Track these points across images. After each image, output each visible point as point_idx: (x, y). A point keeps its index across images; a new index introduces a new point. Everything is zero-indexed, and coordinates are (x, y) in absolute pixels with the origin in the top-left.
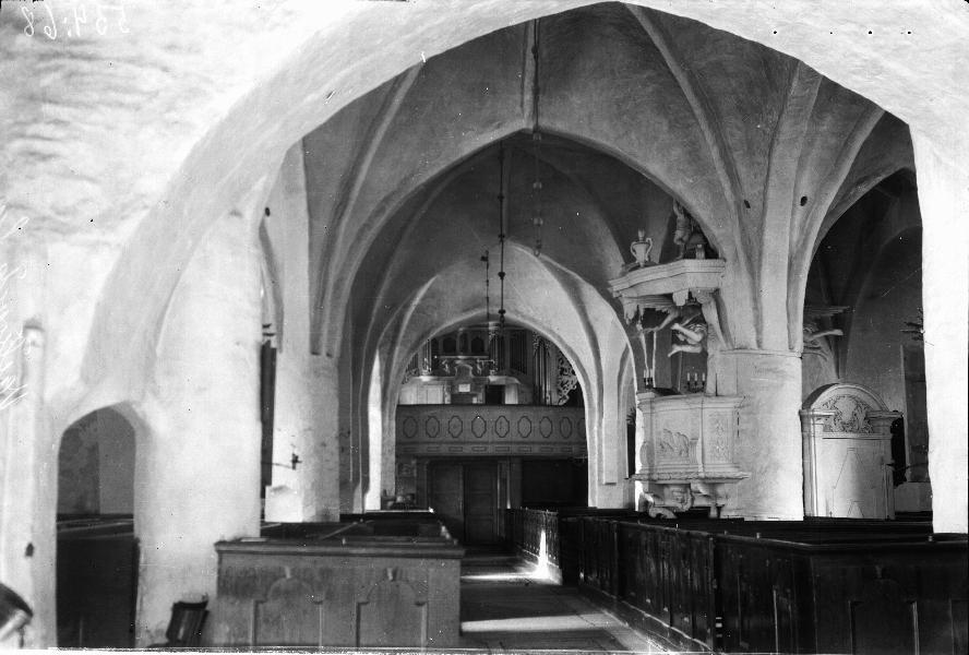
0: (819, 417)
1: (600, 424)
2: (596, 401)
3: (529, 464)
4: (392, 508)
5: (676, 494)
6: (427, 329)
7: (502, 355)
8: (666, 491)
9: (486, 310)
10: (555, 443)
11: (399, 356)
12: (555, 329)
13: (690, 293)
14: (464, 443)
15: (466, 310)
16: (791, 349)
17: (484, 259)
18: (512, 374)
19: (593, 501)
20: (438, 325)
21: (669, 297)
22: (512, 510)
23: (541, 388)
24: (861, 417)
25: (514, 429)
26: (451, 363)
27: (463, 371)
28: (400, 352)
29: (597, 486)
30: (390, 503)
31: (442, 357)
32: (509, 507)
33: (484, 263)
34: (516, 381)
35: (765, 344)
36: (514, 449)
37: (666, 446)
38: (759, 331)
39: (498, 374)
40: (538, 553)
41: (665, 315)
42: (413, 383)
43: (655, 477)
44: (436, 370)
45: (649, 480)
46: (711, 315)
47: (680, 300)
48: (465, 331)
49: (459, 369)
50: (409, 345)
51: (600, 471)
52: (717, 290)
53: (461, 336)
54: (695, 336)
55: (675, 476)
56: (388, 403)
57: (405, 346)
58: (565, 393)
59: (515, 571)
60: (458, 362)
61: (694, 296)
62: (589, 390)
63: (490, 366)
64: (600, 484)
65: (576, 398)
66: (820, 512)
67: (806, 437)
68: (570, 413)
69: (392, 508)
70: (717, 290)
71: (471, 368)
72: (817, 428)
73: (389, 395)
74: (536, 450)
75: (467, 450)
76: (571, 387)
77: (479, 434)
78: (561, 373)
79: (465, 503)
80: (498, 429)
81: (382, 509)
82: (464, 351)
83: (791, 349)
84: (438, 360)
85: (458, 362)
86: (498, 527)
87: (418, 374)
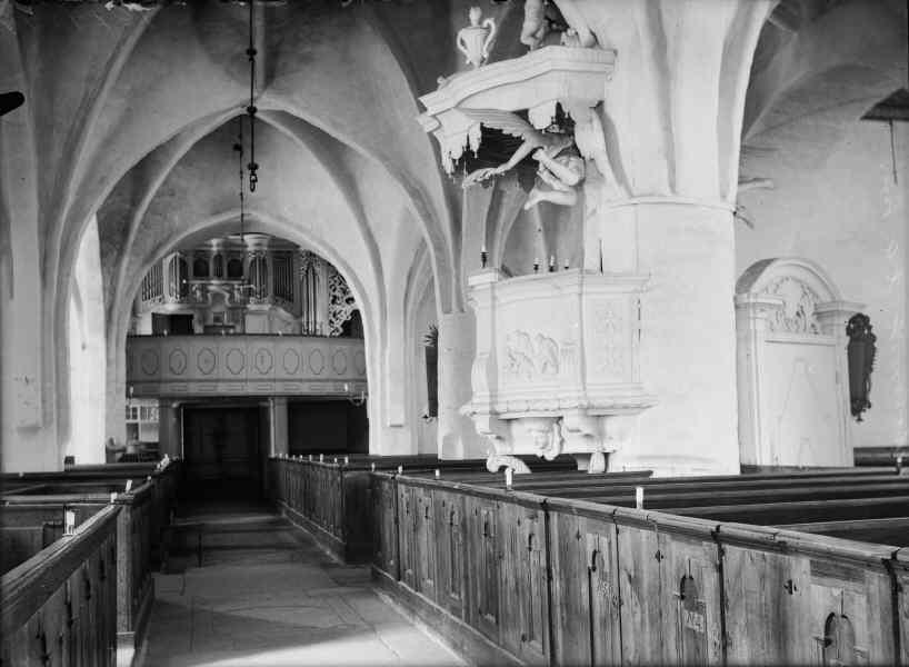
0: (763, 307)
1: (383, 354)
2: (377, 327)
4: (121, 460)
5: (534, 434)
7: (263, 279)
8: (515, 427)
10: (327, 380)
11: (128, 269)
12: (327, 239)
13: (559, 106)
14: (217, 381)
15: (216, 213)
16: (724, 197)
17: (238, 148)
20: (178, 232)
21: (523, 114)
24: (809, 311)
26: (204, 289)
28: (130, 262)
30: (119, 455)
31: (192, 282)
33: (238, 153)
35: (681, 184)
36: (279, 388)
37: (519, 358)
38: (672, 169)
41: (519, 142)
43: (499, 408)
45: (491, 413)
46: (589, 138)
47: (543, 118)
48: (219, 251)
51: (383, 411)
52: (600, 104)
53: (216, 257)
54: (568, 172)
55: (538, 405)
56: (114, 328)
57: (137, 255)
58: (338, 324)
61: (565, 109)
62: (369, 313)
63: (249, 293)
64: (384, 427)
65: (352, 328)
66: (763, 459)
67: (743, 338)
68: (345, 346)
70: (600, 104)
72: (760, 325)
73: (115, 319)
74: (305, 389)
76: (344, 318)
78: (333, 302)
80: (259, 364)
81: (108, 461)
82: (219, 275)
83: (724, 197)
84: (186, 286)
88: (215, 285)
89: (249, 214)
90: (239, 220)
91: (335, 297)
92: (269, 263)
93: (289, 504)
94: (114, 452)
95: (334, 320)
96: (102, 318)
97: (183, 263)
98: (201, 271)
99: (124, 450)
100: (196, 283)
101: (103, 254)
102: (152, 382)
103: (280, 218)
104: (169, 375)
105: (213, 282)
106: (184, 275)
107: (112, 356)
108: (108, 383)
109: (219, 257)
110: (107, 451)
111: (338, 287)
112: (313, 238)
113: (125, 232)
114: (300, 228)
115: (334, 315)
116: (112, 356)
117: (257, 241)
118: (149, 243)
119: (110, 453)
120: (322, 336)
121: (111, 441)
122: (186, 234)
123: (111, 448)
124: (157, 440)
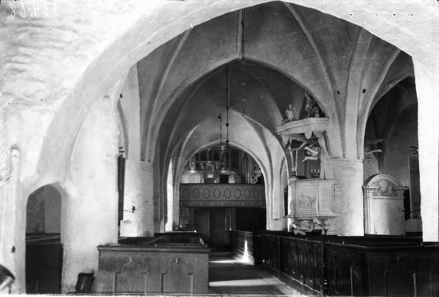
0: (371, 189)
1: (272, 192)
2: (270, 182)
3: (239, 210)
4: (178, 230)
5: (306, 224)
6: (194, 149)
7: (227, 161)
8: (302, 223)
9: (220, 141)
10: (251, 201)
11: (181, 162)
12: (251, 149)
13: (313, 133)
14: (210, 201)
15: (211, 141)
16: (358, 158)
17: (219, 117)
18: (232, 170)
19: (269, 227)
20: (198, 147)
21: (303, 134)
22: (232, 231)
23: (245, 176)
24: (390, 189)
25: (233, 195)
26: (205, 165)
27: (210, 168)
28: (181, 159)
29: (270, 220)
30: (177, 228)
31: (200, 162)
32: (230, 230)
33: (219, 119)
34: (234, 173)
35: (347, 156)
36: (233, 204)
37: (302, 202)
38: (344, 150)
39: (226, 169)
40: (244, 251)
41: (301, 143)
42: (187, 173)
43: (297, 216)
44: (198, 168)
45: (294, 217)
46: (322, 143)
47: (308, 136)
48: (210, 150)
49: (208, 168)
50: (185, 156)
51: (272, 214)
52: (325, 132)
53: (209, 152)
54: (315, 153)
55: (306, 216)
56: (176, 183)
57: (184, 157)
58: (256, 178)
59: (233, 259)
60: (207, 164)
61: (314, 134)
62: (267, 177)
63: (222, 166)
64: (272, 220)
65: (261, 181)
66: (372, 232)
67: (365, 198)
68: (258, 187)
69: (178, 230)
70: (325, 132)
71: (213, 167)
72: (370, 194)
73: (176, 179)
74: (243, 204)
75: (212, 204)
76: (259, 176)
77: (217, 197)
78: (254, 169)
79: (211, 228)
80: (226, 195)
81: (173, 231)
82: (210, 159)
83: (358, 158)
84: (198, 163)
85: (207, 164)
86: (226, 239)
87: (189, 169)
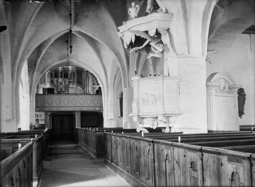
0: (214, 86)
1: (107, 99)
2: (106, 92)
4: (34, 129)
5: (150, 122)
7: (74, 78)
8: (145, 120)
10: (92, 107)
11: (36, 75)
12: (92, 67)
13: (157, 30)
14: (61, 107)
15: (61, 60)
16: (203, 55)
17: (67, 41)
20: (50, 65)
21: (147, 32)
24: (227, 87)
26: (57, 81)
28: (37, 74)
30: (33, 128)
31: (54, 79)
33: (67, 43)
35: (191, 52)
36: (78, 109)
37: (146, 101)
38: (189, 47)
41: (146, 40)
43: (140, 114)
45: (138, 116)
46: (165, 39)
47: (152, 33)
48: (61, 70)
51: (108, 115)
52: (168, 29)
53: (61, 72)
54: (159, 48)
55: (151, 114)
56: (32, 92)
57: (38, 71)
58: (95, 91)
61: (159, 31)
62: (104, 88)
63: (70, 82)
64: (108, 120)
65: (99, 92)
66: (214, 129)
67: (208, 95)
68: (97, 97)
70: (168, 29)
72: (213, 91)
73: (32, 89)
74: (85, 109)
76: (97, 89)
78: (94, 85)
80: (73, 102)
81: (30, 129)
82: (61, 77)
83: (203, 55)
84: (52, 80)
88: (60, 80)
89: (70, 60)
90: (67, 62)
91: (94, 83)
92: (76, 74)
93: (81, 141)
94: (32, 127)
95: (94, 90)
96: (28, 89)
97: (51, 74)
98: (56, 76)
99: (35, 126)
100: (55, 79)
101: (29, 71)
102: (43, 107)
103: (79, 61)
104: (47, 105)
105: (60, 79)
106: (52, 77)
107: (32, 100)
108: (30, 107)
109: (61, 72)
110: (30, 126)
111: (95, 81)
112: (88, 67)
113: (35, 65)
114: (84, 64)
115: (94, 88)
116: (32, 100)
117: (72, 68)
118: (42, 68)
119: (31, 127)
120: (90, 94)
121: (31, 124)
122: (52, 66)
123: (31, 126)
124: (44, 123)
